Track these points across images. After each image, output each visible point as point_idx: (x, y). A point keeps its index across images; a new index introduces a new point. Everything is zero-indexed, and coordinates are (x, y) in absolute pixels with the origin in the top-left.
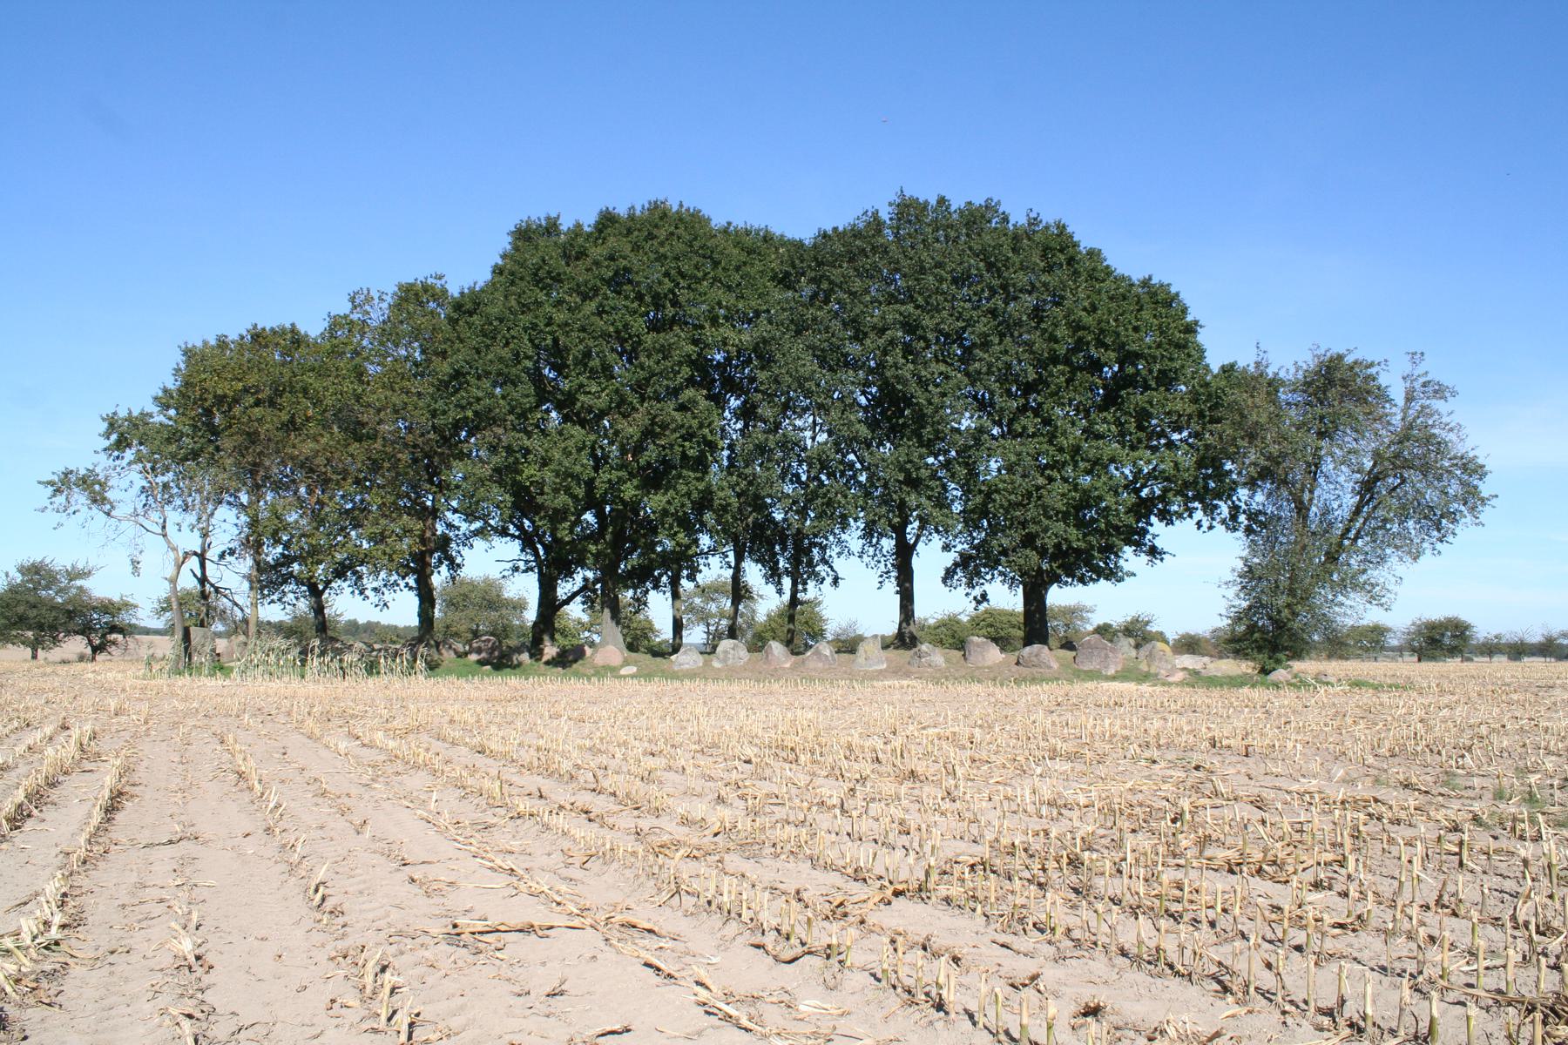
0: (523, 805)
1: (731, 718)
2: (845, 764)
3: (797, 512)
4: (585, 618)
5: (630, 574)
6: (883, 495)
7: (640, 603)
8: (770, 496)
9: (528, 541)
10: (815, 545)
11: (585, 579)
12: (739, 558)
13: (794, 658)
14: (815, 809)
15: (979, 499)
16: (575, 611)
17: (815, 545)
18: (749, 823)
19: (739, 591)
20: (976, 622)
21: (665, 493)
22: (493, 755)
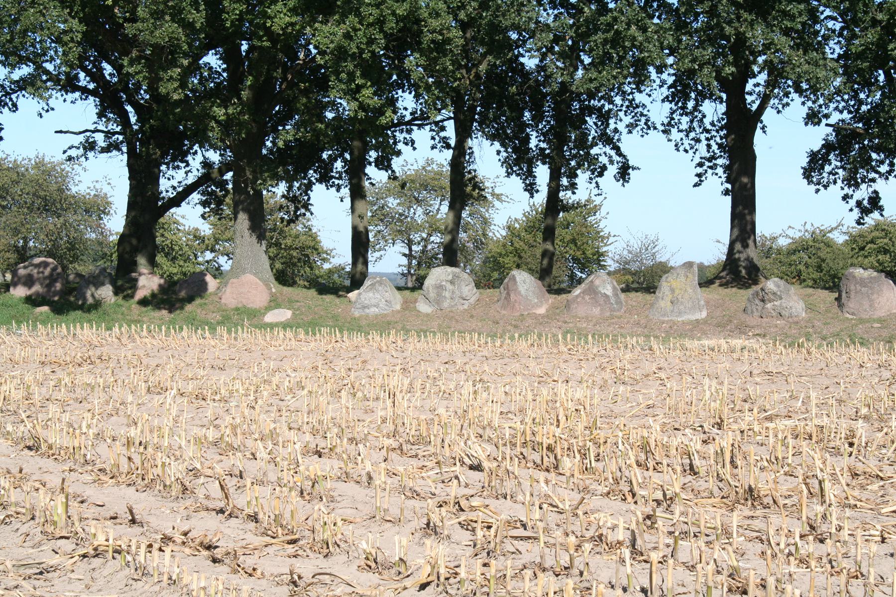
0: (103, 534)
1: (447, 395)
2: (637, 475)
3: (562, 55)
4: (206, 229)
5: (282, 156)
6: (708, 27)
7: (299, 204)
8: (516, 28)
9: (110, 100)
10: (591, 110)
11: (206, 164)
12: (463, 132)
13: (552, 299)
14: (587, 546)
15: (872, 35)
16: (190, 216)
17: (591, 110)
18: (479, 569)
19: (463, 188)
20: (859, 245)
21: (341, 21)
22: (52, 453)
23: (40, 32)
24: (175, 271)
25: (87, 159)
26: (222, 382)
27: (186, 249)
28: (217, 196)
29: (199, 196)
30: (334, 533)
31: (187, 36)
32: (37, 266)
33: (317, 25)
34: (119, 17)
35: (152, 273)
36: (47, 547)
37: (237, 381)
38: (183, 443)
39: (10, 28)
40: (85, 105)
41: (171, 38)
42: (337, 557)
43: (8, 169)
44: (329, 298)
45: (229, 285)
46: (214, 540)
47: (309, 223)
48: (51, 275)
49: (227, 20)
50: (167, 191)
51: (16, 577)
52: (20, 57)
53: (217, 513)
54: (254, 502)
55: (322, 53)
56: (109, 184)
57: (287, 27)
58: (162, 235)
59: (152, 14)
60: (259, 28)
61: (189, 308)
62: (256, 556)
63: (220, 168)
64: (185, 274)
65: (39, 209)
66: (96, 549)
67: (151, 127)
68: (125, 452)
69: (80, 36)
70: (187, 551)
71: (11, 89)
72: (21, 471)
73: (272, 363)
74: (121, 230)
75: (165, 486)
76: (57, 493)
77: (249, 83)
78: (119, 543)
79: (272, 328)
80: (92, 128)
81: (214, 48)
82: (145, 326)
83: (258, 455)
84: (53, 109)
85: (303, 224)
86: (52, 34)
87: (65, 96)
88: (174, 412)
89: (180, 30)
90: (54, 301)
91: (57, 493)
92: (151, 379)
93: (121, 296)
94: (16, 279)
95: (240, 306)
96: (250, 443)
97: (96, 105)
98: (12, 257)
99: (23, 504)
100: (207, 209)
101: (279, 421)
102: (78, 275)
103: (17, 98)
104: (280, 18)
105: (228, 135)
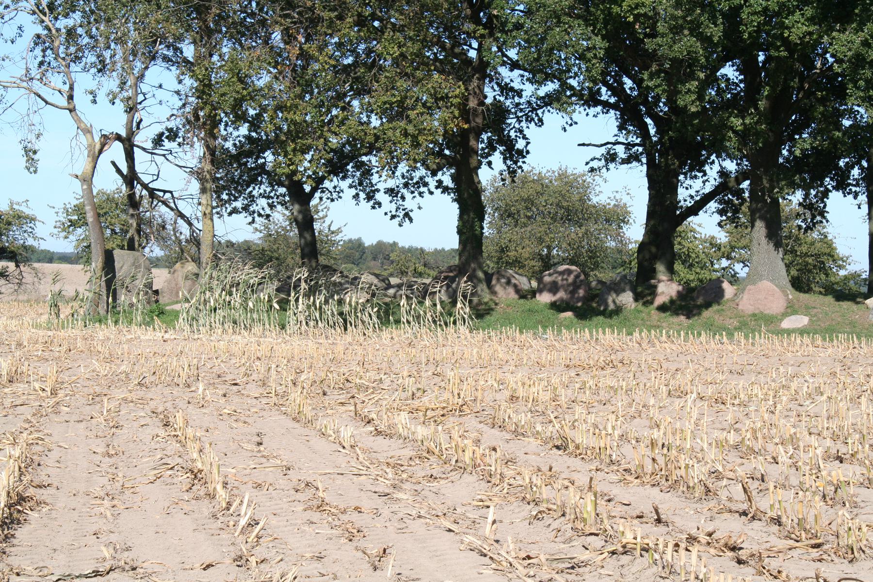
0: (631, 533)
4: (722, 237)
5: (798, 164)
7: (815, 211)
9: (630, 113)
11: (723, 173)
16: (707, 225)
22: (579, 452)
23: (565, 50)
24: (692, 277)
25: (608, 169)
26: (740, 386)
27: (702, 256)
28: (733, 205)
29: (716, 205)
30: (859, 538)
31: (705, 49)
33: (834, 34)
34: (640, 33)
35: (671, 280)
36: (578, 542)
37: (756, 386)
38: (705, 446)
39: (536, 47)
40: (607, 119)
41: (689, 53)
42: (863, 563)
43: (533, 181)
44: (846, 305)
45: (746, 292)
46: (738, 542)
47: (825, 230)
48: (575, 282)
49: (745, 32)
50: (685, 201)
51: (550, 571)
52: (547, 74)
53: (740, 515)
54: (777, 506)
55: (839, 61)
56: (628, 194)
57: (804, 37)
58: (680, 243)
59: (671, 29)
60: (777, 39)
61: (706, 314)
62: (781, 559)
63: (736, 177)
64: (701, 281)
65: (562, 219)
66: (624, 547)
67: (670, 138)
68: (649, 453)
69: (602, 52)
70: (713, 551)
71: (537, 105)
72: (550, 469)
73: (790, 369)
74: (640, 238)
75: (688, 487)
76: (585, 491)
77: (766, 93)
78: (646, 541)
79: (789, 335)
80: (613, 140)
81: (731, 60)
82: (664, 331)
83: (780, 459)
84: (576, 123)
85: (818, 231)
86: (576, 52)
87: (588, 110)
88: (695, 415)
89: (698, 44)
90: (577, 307)
91: (585, 491)
92: (672, 382)
93: (641, 302)
94: (541, 286)
95: (757, 312)
96: (770, 447)
97: (617, 118)
98: (537, 264)
99: (554, 501)
100: (724, 218)
101: (799, 426)
102: (600, 282)
103: (543, 113)
104: (798, 28)
105: (745, 145)
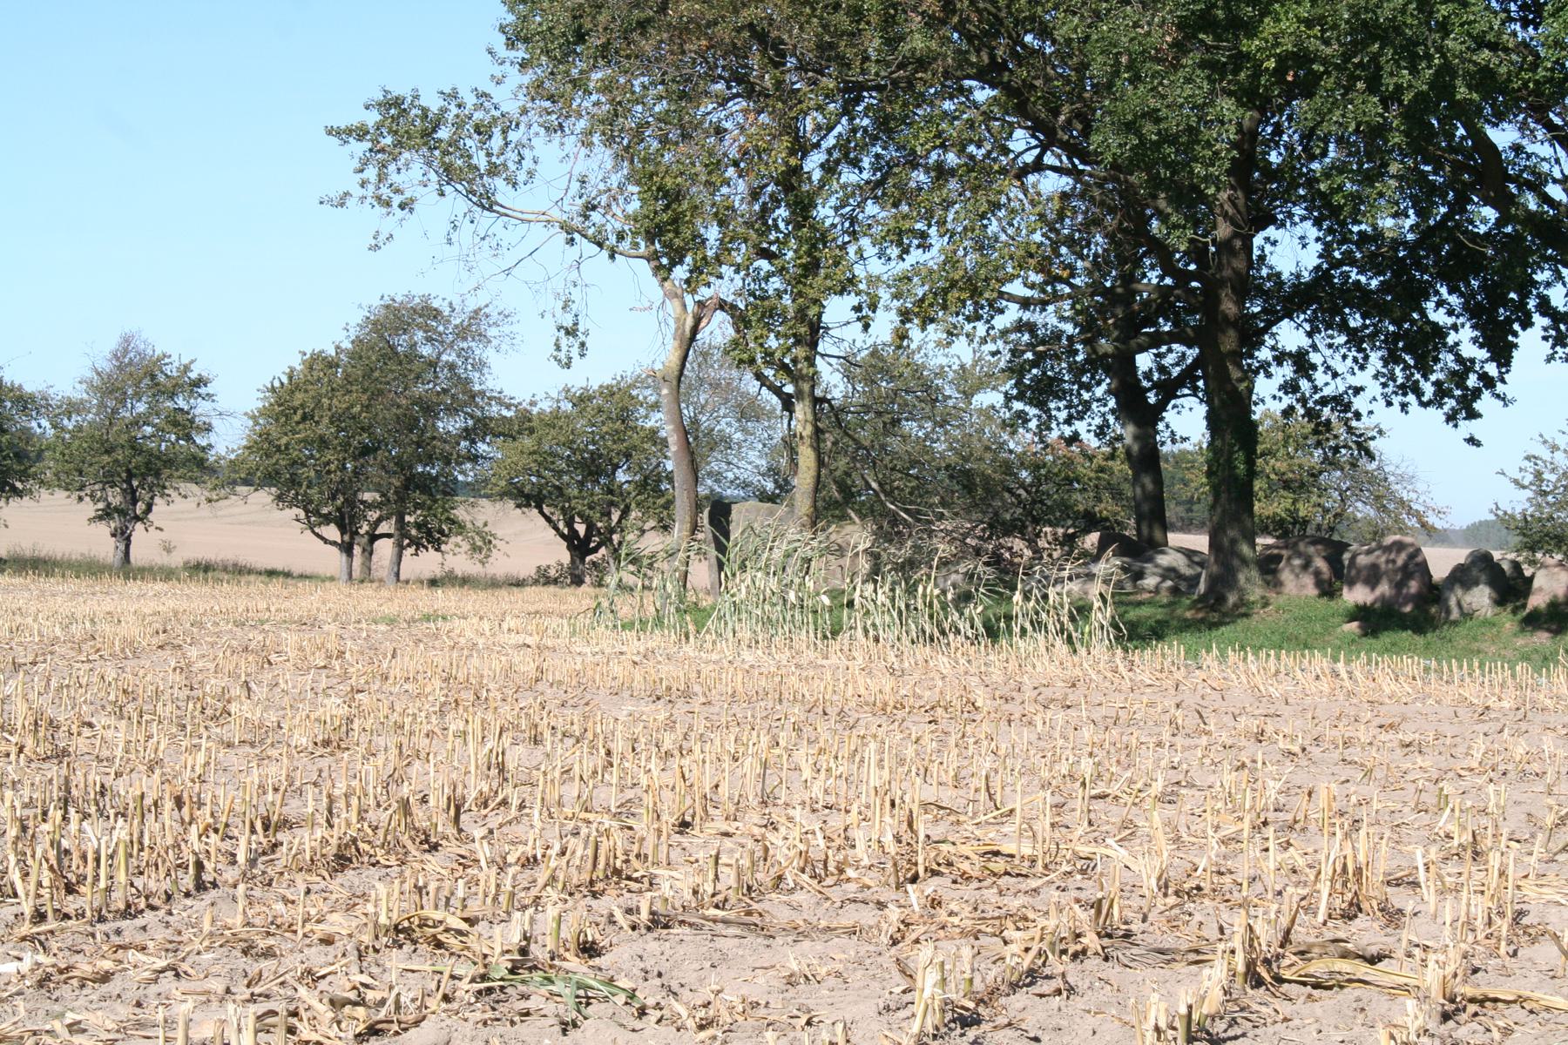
32: (1388, 549)
48: (1405, 566)
